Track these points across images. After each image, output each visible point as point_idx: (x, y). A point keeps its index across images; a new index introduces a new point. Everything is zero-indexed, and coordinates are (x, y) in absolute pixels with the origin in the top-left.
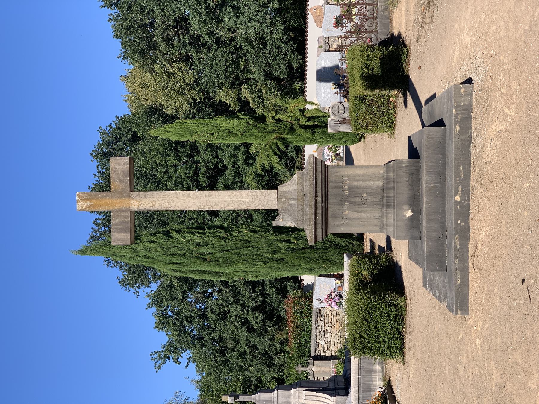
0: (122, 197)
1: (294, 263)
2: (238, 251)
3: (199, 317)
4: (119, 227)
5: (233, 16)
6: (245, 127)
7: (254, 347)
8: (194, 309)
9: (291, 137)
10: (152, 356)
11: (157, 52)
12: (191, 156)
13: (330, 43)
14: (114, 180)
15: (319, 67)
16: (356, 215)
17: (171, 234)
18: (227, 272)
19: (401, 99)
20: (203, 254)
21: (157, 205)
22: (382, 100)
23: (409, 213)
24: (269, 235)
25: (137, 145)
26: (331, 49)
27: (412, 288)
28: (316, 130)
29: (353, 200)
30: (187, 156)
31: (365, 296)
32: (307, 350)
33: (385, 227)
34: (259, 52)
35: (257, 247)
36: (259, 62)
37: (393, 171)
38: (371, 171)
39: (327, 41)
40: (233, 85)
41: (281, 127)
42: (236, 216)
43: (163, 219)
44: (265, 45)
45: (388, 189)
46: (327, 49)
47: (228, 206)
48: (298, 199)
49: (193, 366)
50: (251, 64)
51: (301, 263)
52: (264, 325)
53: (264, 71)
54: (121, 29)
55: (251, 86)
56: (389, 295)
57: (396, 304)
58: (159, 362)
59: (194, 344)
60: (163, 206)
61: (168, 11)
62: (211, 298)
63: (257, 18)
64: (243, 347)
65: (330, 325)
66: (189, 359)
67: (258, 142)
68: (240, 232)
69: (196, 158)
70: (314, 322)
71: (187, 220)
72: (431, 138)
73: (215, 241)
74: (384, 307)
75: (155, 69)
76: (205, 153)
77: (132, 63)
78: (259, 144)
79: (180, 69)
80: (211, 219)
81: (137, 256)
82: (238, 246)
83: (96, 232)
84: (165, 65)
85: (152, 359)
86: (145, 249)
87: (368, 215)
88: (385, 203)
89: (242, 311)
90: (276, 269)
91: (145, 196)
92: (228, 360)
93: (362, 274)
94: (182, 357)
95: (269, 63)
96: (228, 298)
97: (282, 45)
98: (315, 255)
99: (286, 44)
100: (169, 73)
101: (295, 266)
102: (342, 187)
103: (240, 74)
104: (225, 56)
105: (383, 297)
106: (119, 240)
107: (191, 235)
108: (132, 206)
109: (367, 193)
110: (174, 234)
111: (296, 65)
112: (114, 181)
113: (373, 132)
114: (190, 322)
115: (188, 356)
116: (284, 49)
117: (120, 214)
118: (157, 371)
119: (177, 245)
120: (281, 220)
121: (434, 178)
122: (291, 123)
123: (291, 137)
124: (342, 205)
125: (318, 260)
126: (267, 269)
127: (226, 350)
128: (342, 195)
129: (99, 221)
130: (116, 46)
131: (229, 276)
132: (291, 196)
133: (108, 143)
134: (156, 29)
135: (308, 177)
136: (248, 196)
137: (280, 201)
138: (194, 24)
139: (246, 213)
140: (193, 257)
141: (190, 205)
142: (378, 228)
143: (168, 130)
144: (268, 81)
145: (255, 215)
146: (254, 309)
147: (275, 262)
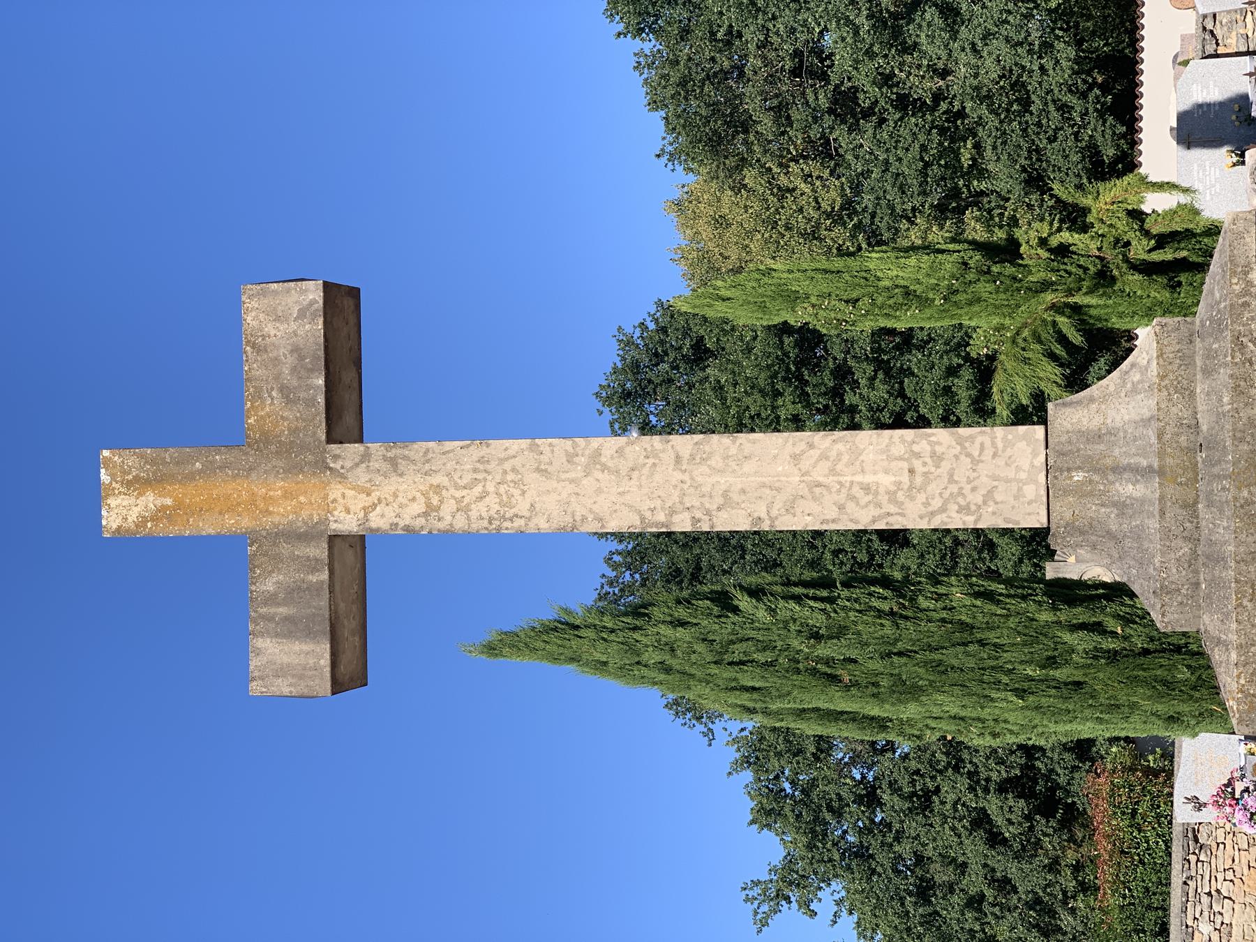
0: (294, 469)
1: (1115, 698)
3: (859, 800)
4: (283, 610)
5: (941, 29)
6: (953, 276)
7: (1004, 885)
8: (848, 781)
9: (1101, 302)
11: (752, 138)
12: (837, 393)
13: (1218, 32)
14: (258, 390)
15: (1186, 105)
17: (736, 602)
18: (904, 717)
20: (828, 662)
21: (447, 509)
24: (1033, 607)
25: (703, 369)
28: (1183, 278)
30: (825, 394)
34: (1011, 121)
35: (995, 645)
39: (1210, 26)
40: (942, 212)
41: (1070, 273)
42: (870, 563)
43: (770, 554)
44: (1026, 103)
46: (1210, 49)
47: (790, 510)
48: (1161, 472)
49: (848, 922)
50: (988, 153)
51: (1140, 696)
52: (1031, 828)
53: (1024, 170)
54: (665, 87)
58: (765, 908)
59: (849, 868)
60: (474, 514)
61: (777, 33)
62: (889, 755)
64: (975, 882)
65: (1230, 875)
66: (839, 903)
69: (850, 398)
70: (1176, 866)
71: (828, 556)
73: (864, 622)
75: (747, 181)
76: (872, 386)
77: (691, 170)
78: (999, 328)
79: (807, 177)
80: (888, 552)
81: (638, 663)
83: (611, 584)
84: (770, 169)
85: (747, 900)
86: (659, 646)
89: (972, 789)
90: (1057, 714)
91: (393, 462)
94: (820, 900)
95: (1038, 151)
97: (1069, 99)
98: (1183, 674)
99: (1084, 96)
100: (779, 188)
101: (1118, 707)
103: (961, 183)
106: (281, 672)
107: (792, 604)
108: (339, 513)
110: (744, 602)
111: (1109, 152)
112: (258, 395)
115: (837, 896)
116: (1078, 109)
117: (285, 549)
118: (760, 931)
119: (752, 634)
120: (1072, 559)
125: (1194, 688)
126: (1028, 713)
127: (932, 888)
129: (617, 558)
130: (653, 128)
131: (909, 731)
132: (1120, 454)
133: (635, 367)
134: (749, 80)
136: (891, 459)
138: (842, 60)
139: (979, 537)
140: (798, 672)
141: (603, 505)
143: (723, 293)
144: (1034, 197)
145: (1001, 542)
146: (1002, 788)
147: (1053, 691)
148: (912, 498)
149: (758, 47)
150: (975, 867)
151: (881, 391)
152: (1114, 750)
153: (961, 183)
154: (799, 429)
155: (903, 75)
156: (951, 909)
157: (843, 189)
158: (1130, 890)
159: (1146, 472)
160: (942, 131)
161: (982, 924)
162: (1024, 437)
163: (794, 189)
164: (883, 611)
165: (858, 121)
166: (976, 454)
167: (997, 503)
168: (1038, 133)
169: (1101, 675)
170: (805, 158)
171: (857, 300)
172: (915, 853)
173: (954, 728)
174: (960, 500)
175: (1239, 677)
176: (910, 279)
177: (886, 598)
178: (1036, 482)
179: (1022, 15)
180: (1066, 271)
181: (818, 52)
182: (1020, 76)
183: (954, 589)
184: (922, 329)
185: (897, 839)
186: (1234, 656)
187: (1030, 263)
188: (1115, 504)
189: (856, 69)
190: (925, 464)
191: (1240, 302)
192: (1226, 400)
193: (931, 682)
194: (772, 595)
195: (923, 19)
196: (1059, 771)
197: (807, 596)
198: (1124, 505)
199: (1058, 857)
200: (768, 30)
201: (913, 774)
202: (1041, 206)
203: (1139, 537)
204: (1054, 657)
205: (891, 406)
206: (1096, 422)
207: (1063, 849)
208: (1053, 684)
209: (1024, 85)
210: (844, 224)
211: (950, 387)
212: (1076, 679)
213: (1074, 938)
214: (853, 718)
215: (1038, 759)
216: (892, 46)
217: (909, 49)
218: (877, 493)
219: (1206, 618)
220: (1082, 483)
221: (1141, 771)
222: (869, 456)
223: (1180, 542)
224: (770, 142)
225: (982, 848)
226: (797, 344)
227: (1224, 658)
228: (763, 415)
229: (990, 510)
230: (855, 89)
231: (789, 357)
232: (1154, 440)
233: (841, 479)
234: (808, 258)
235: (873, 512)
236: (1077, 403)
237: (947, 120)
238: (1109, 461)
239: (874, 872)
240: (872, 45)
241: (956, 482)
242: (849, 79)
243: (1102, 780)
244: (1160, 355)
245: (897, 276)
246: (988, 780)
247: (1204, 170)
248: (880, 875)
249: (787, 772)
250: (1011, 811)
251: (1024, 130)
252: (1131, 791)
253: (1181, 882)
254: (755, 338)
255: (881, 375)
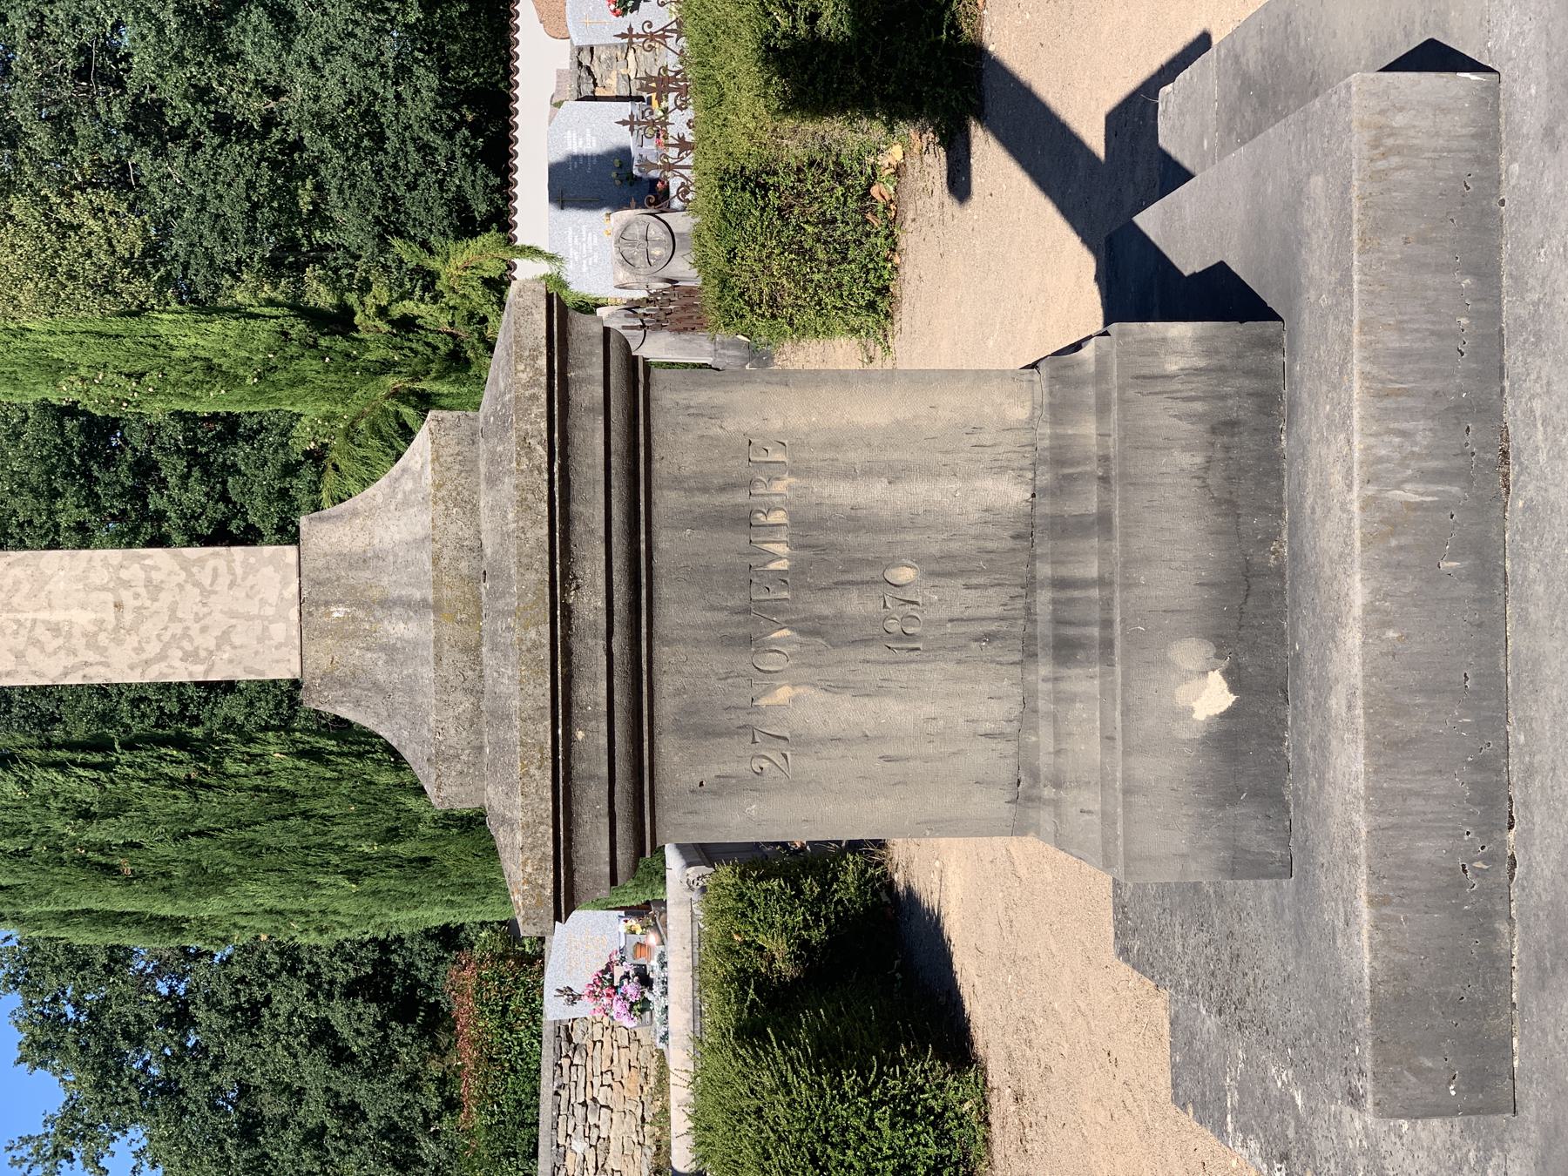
1: (469, 875)
2: (248, 835)
3: (165, 1021)
5: (272, 37)
6: (269, 349)
7: (350, 1112)
8: (151, 997)
9: (454, 390)
10: (13, 1152)
11: (21, 155)
12: (138, 494)
13: (595, 69)
15: (559, 156)
16: (847, 712)
18: (205, 915)
19: (936, 164)
20: (102, 848)
22: (839, 191)
23: (1212, 697)
24: (370, 767)
26: (599, 92)
27: (1029, 1043)
29: (826, 610)
30: (122, 495)
31: (791, 1077)
32: (524, 1133)
33: (1048, 792)
34: (361, 160)
35: (323, 817)
36: (359, 194)
37: (1102, 409)
38: (951, 405)
39: (586, 62)
41: (416, 352)
44: (379, 139)
45: (1065, 528)
46: (587, 89)
48: (437, 608)
50: (333, 197)
52: (385, 1038)
53: (378, 221)
55: (336, 270)
56: (900, 1062)
57: (937, 1106)
59: (152, 1110)
61: (55, 22)
62: (206, 960)
63: (352, 45)
64: (314, 1112)
65: (607, 1079)
67: (325, 407)
68: (253, 756)
69: (155, 502)
70: (546, 1074)
71: (125, 706)
72: (1397, 151)
73: (152, 792)
74: (884, 1126)
75: (14, 211)
76: (185, 487)
78: (330, 417)
79: (97, 212)
80: (207, 701)
82: (245, 815)
84: (46, 198)
85: (14, 1162)
87: (929, 709)
88: (1044, 629)
89: (311, 995)
90: (399, 900)
92: (265, 1155)
93: (761, 948)
94: (113, 1154)
95: (394, 199)
96: (263, 956)
99: (449, 135)
100: (59, 224)
101: (472, 886)
102: (745, 520)
103: (300, 232)
104: (248, 171)
105: (880, 1074)
107: (53, 774)
109: (919, 560)
111: (481, 208)
113: (802, 331)
114: (137, 1041)
115: (136, 1147)
121: (1423, 440)
122: (454, 336)
123: (454, 390)
124: (749, 641)
126: (363, 900)
127: (260, 1124)
128: (750, 574)
131: (211, 932)
132: (389, 583)
134: (16, 79)
135: (511, 446)
136: (89, 588)
137: (319, 618)
138: (143, 64)
140: (61, 862)
142: (995, 803)
146: (350, 991)
148: (120, 642)
149: (30, 38)
150: (315, 1093)
151: (196, 493)
152: (483, 935)
153: (300, 232)
154: (84, 544)
155: (223, 90)
156: (283, 1150)
157: (146, 230)
158: (499, 1105)
159: (419, 607)
160: (275, 165)
161: (323, 1164)
162: (271, 561)
163: (80, 226)
164: (177, 780)
165: (165, 143)
166: (207, 582)
167: (235, 648)
168: (395, 178)
169: (452, 848)
170: (95, 186)
171: (143, 374)
172: (239, 1082)
173: (269, 925)
174: (186, 644)
175: (525, 864)
176: (206, 354)
177: (181, 762)
178: (287, 619)
179: (372, 28)
180: (411, 349)
181: (110, 51)
182: (371, 104)
183: (272, 748)
184: (251, 415)
185: (215, 1067)
186: (519, 837)
187: (367, 336)
188: (383, 648)
189: (161, 76)
190: (137, 596)
191: (527, 394)
192: (510, 516)
193: (240, 868)
194: (25, 762)
195: (249, 22)
196: (420, 965)
197: (73, 762)
198: (394, 648)
199: (418, 1070)
200: (43, 17)
201: (237, 982)
202: (399, 268)
203: (411, 690)
204: (396, 829)
205: (210, 513)
206: (359, 544)
207: (424, 1060)
208: (394, 862)
209: (376, 116)
210: (147, 276)
211: (287, 490)
212: (423, 854)
213: (437, 1169)
214: (138, 920)
215: (395, 951)
216: (208, 52)
217: (229, 58)
218: (70, 635)
219: (490, 790)
220: (343, 621)
221: (514, 959)
222: (59, 585)
223: (459, 695)
224: (47, 162)
225: (324, 1068)
226: (83, 429)
227: (509, 840)
228: (36, 522)
229: (226, 656)
230: (163, 102)
231: (72, 447)
232: (429, 566)
233: (19, 616)
234: (92, 313)
235: (66, 661)
236: (336, 517)
237: (281, 152)
238: (375, 593)
239: (184, 1111)
240: (182, 48)
241: (180, 620)
242: (153, 89)
243: (467, 973)
244: (436, 458)
245: (196, 345)
246: (332, 982)
247: (580, 236)
248: (192, 1114)
249: (69, 992)
250: (360, 1019)
251: (378, 173)
252: (502, 983)
253: (551, 1093)
254: (25, 420)
255: (196, 473)
